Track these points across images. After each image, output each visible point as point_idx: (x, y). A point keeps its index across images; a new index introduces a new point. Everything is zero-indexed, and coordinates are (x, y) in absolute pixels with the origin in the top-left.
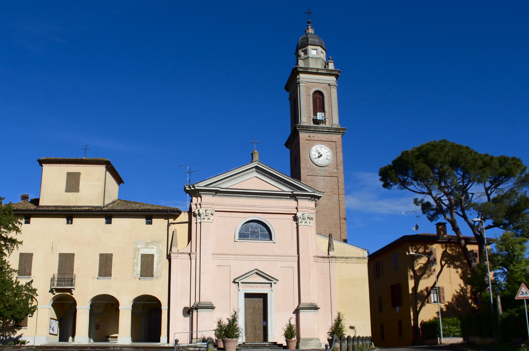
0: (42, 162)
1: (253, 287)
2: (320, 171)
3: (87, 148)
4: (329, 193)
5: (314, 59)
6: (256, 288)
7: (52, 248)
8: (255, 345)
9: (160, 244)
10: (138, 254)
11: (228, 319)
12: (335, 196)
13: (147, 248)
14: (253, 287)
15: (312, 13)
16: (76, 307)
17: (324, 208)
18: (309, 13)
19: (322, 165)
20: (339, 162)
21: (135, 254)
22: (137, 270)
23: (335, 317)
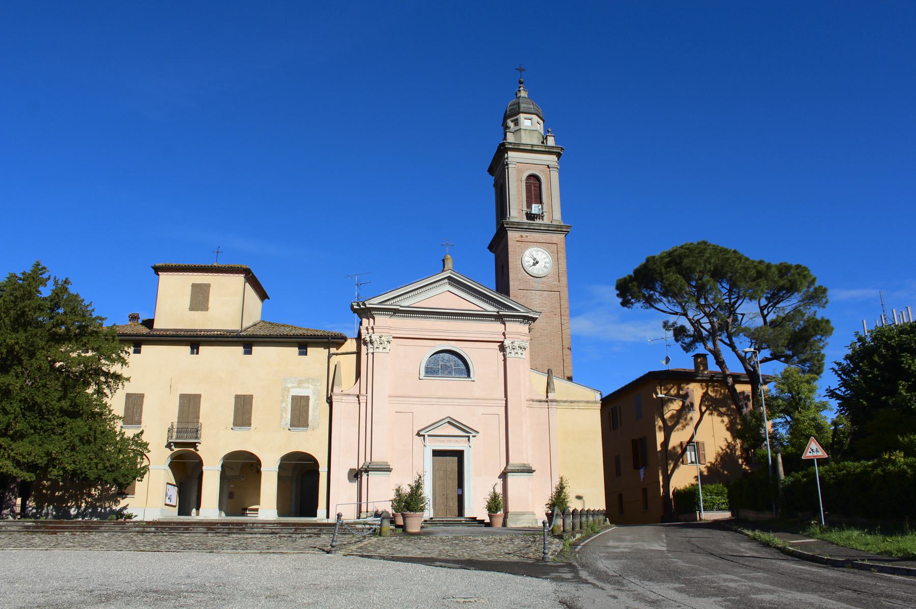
0: (157, 270)
1: (444, 442)
13: (300, 387)
14: (444, 442)
21: (283, 396)
23: (556, 482)
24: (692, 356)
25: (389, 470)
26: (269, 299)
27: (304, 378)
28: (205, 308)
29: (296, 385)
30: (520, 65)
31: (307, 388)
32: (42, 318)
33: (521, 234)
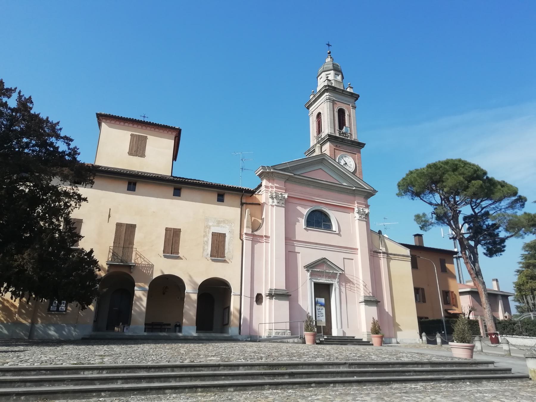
0: (101, 117)
1: (320, 276)
3: (143, 115)
7: (109, 216)
10: (209, 232)
11: (58, 123)
13: (219, 226)
14: (320, 276)
15: (331, 46)
18: (329, 45)
21: (205, 232)
22: (207, 249)
24: (414, 235)
27: (222, 220)
28: (143, 155)
29: (216, 224)
31: (224, 227)
32: (23, 100)
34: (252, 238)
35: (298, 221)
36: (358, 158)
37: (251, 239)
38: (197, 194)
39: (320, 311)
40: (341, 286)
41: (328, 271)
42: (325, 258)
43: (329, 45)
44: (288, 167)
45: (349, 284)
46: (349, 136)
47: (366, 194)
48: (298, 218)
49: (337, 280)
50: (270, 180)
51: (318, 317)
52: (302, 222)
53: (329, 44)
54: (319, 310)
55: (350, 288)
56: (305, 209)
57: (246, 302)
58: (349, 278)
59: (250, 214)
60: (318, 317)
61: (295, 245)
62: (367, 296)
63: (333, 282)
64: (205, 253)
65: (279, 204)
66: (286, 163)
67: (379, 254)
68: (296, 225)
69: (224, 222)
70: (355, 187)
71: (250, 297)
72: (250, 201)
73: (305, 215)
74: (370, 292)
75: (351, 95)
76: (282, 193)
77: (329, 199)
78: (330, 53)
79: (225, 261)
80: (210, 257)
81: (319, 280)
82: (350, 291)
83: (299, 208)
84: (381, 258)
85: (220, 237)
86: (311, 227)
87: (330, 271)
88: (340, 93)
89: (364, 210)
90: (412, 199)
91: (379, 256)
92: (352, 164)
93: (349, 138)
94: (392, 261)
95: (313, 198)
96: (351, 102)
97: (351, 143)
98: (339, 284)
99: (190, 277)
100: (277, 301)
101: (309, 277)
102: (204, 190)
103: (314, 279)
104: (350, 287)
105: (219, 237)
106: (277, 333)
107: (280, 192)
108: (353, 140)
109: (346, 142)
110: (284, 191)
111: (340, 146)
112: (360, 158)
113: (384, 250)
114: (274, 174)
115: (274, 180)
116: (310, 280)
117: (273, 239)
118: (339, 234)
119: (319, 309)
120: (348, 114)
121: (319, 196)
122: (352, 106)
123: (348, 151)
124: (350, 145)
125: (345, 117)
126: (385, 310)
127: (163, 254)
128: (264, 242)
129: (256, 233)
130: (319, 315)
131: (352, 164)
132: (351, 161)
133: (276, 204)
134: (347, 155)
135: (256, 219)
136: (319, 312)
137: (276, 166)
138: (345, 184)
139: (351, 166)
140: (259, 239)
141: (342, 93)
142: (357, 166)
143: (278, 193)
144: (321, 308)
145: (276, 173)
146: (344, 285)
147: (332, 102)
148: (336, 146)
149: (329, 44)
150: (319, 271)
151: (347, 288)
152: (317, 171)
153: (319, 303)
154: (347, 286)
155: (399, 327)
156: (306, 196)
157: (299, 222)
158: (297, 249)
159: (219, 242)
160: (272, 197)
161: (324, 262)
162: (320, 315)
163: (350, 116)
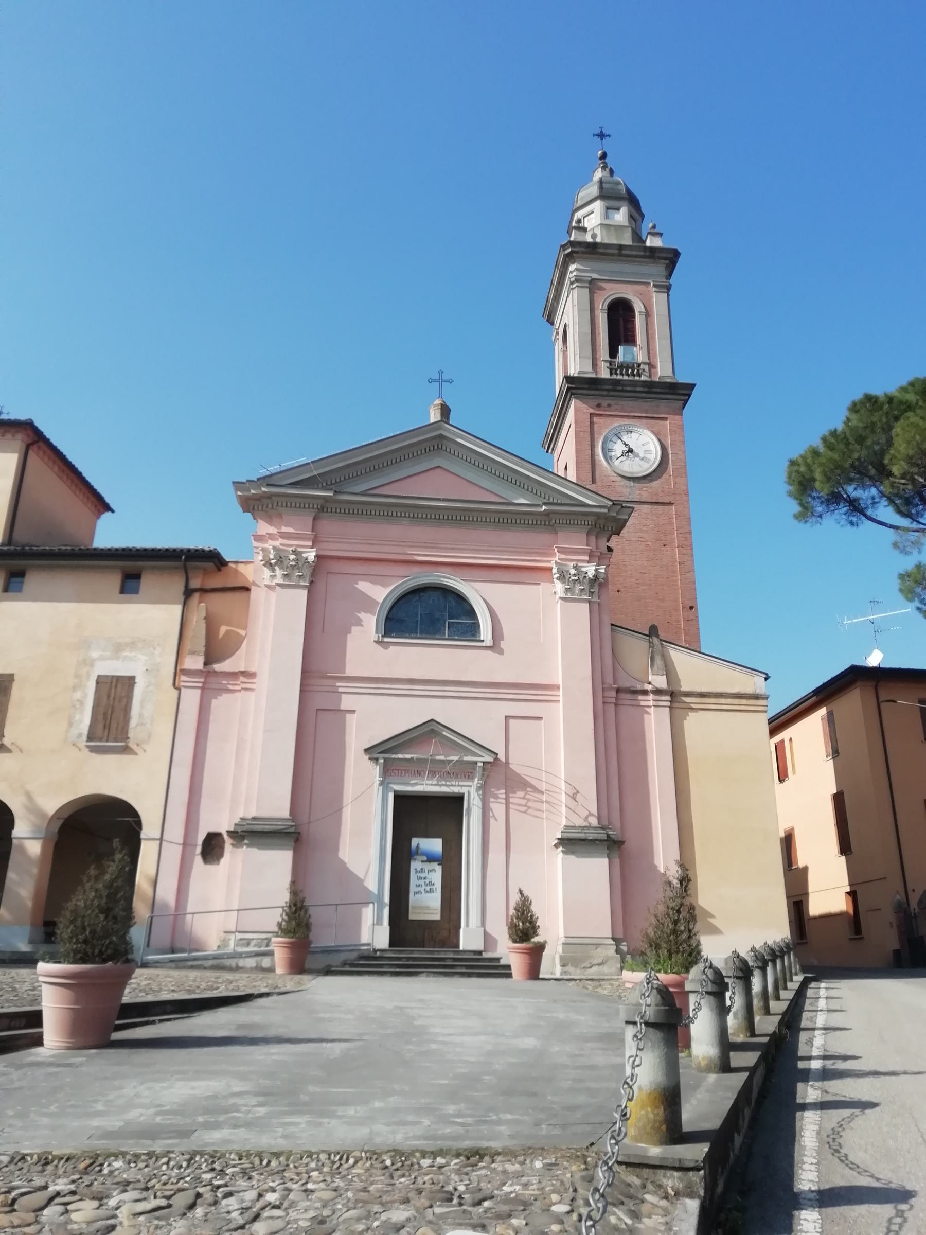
2: (628, 490)
4: (650, 543)
5: (612, 229)
6: (407, 775)
8: (408, 959)
9: (155, 649)
12: (667, 551)
13: (118, 658)
15: (610, 136)
16: (10, 833)
17: (638, 580)
18: (601, 136)
19: (632, 473)
20: (678, 467)
22: (81, 721)
23: (515, 898)
25: (781, 780)
26: (113, 511)
30: (601, 127)
33: (599, 401)
34: (202, 680)
35: (359, 623)
36: (673, 429)
37: (200, 685)
38: (65, 580)
39: (423, 875)
40: (492, 800)
41: (442, 758)
42: (432, 720)
43: (601, 136)
44: (315, 475)
45: (520, 794)
46: (644, 370)
47: (591, 520)
48: (359, 615)
49: (475, 783)
50: (282, 517)
51: (415, 893)
52: (370, 623)
53: (601, 132)
54: (419, 875)
55: (525, 805)
56: (383, 587)
57: (173, 854)
58: (524, 777)
59: (205, 618)
60: (415, 893)
61: (340, 690)
62: (576, 827)
63: (464, 790)
64: (74, 731)
65: (290, 580)
66: (309, 463)
67: (640, 697)
68: (349, 635)
69: (133, 645)
70: (545, 504)
71: (181, 841)
72: (216, 581)
73: (381, 601)
74: (590, 814)
75: (647, 254)
76: (580, 564)
77: (464, 549)
78: (604, 156)
79: (126, 750)
80: (87, 741)
81: (416, 784)
82: (525, 812)
83: (364, 586)
84: (647, 709)
85: (119, 686)
86: (407, 635)
87: (451, 758)
88: (613, 255)
89: (583, 569)
90: (852, 523)
91: (642, 703)
92: (652, 448)
93: (643, 378)
94: (692, 715)
95: (409, 552)
96: (650, 276)
97: (646, 389)
98: (484, 794)
99: (29, 796)
100: (572, 858)
101: (378, 779)
102: (76, 568)
103: (394, 783)
104: (523, 802)
105: (116, 687)
106: (244, 941)
107: (291, 546)
108: (658, 380)
109: (629, 389)
110: (587, 558)
111: (609, 405)
112: (679, 429)
113: (660, 681)
114: (274, 498)
115: (280, 516)
116: (381, 788)
117: (262, 683)
118: (495, 647)
119: (422, 870)
120: (643, 310)
121: (433, 545)
122: (655, 286)
123: (640, 415)
124: (644, 395)
125: (633, 322)
126: (654, 868)
127: (85, 743)
128: (651, 707)
129: (217, 667)
130: (417, 889)
131: (652, 448)
132: (648, 443)
133: (281, 581)
134: (636, 426)
135: (234, 629)
136: (419, 878)
137: (274, 477)
138: (522, 501)
139: (648, 456)
140: (224, 682)
141: (620, 255)
142: (670, 452)
143: (565, 565)
144: (428, 866)
145: (278, 495)
146: (504, 796)
147: (586, 287)
148: (599, 406)
149: (601, 132)
150: (412, 759)
151: (511, 806)
152: (426, 474)
153: (423, 854)
154: (511, 800)
155: (711, 920)
156: (386, 549)
157: (362, 625)
158: (347, 702)
159: (114, 699)
160: (269, 565)
161: (432, 731)
162: (424, 887)
163: (647, 314)
